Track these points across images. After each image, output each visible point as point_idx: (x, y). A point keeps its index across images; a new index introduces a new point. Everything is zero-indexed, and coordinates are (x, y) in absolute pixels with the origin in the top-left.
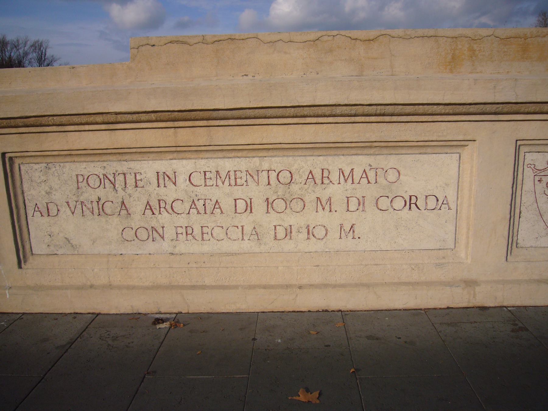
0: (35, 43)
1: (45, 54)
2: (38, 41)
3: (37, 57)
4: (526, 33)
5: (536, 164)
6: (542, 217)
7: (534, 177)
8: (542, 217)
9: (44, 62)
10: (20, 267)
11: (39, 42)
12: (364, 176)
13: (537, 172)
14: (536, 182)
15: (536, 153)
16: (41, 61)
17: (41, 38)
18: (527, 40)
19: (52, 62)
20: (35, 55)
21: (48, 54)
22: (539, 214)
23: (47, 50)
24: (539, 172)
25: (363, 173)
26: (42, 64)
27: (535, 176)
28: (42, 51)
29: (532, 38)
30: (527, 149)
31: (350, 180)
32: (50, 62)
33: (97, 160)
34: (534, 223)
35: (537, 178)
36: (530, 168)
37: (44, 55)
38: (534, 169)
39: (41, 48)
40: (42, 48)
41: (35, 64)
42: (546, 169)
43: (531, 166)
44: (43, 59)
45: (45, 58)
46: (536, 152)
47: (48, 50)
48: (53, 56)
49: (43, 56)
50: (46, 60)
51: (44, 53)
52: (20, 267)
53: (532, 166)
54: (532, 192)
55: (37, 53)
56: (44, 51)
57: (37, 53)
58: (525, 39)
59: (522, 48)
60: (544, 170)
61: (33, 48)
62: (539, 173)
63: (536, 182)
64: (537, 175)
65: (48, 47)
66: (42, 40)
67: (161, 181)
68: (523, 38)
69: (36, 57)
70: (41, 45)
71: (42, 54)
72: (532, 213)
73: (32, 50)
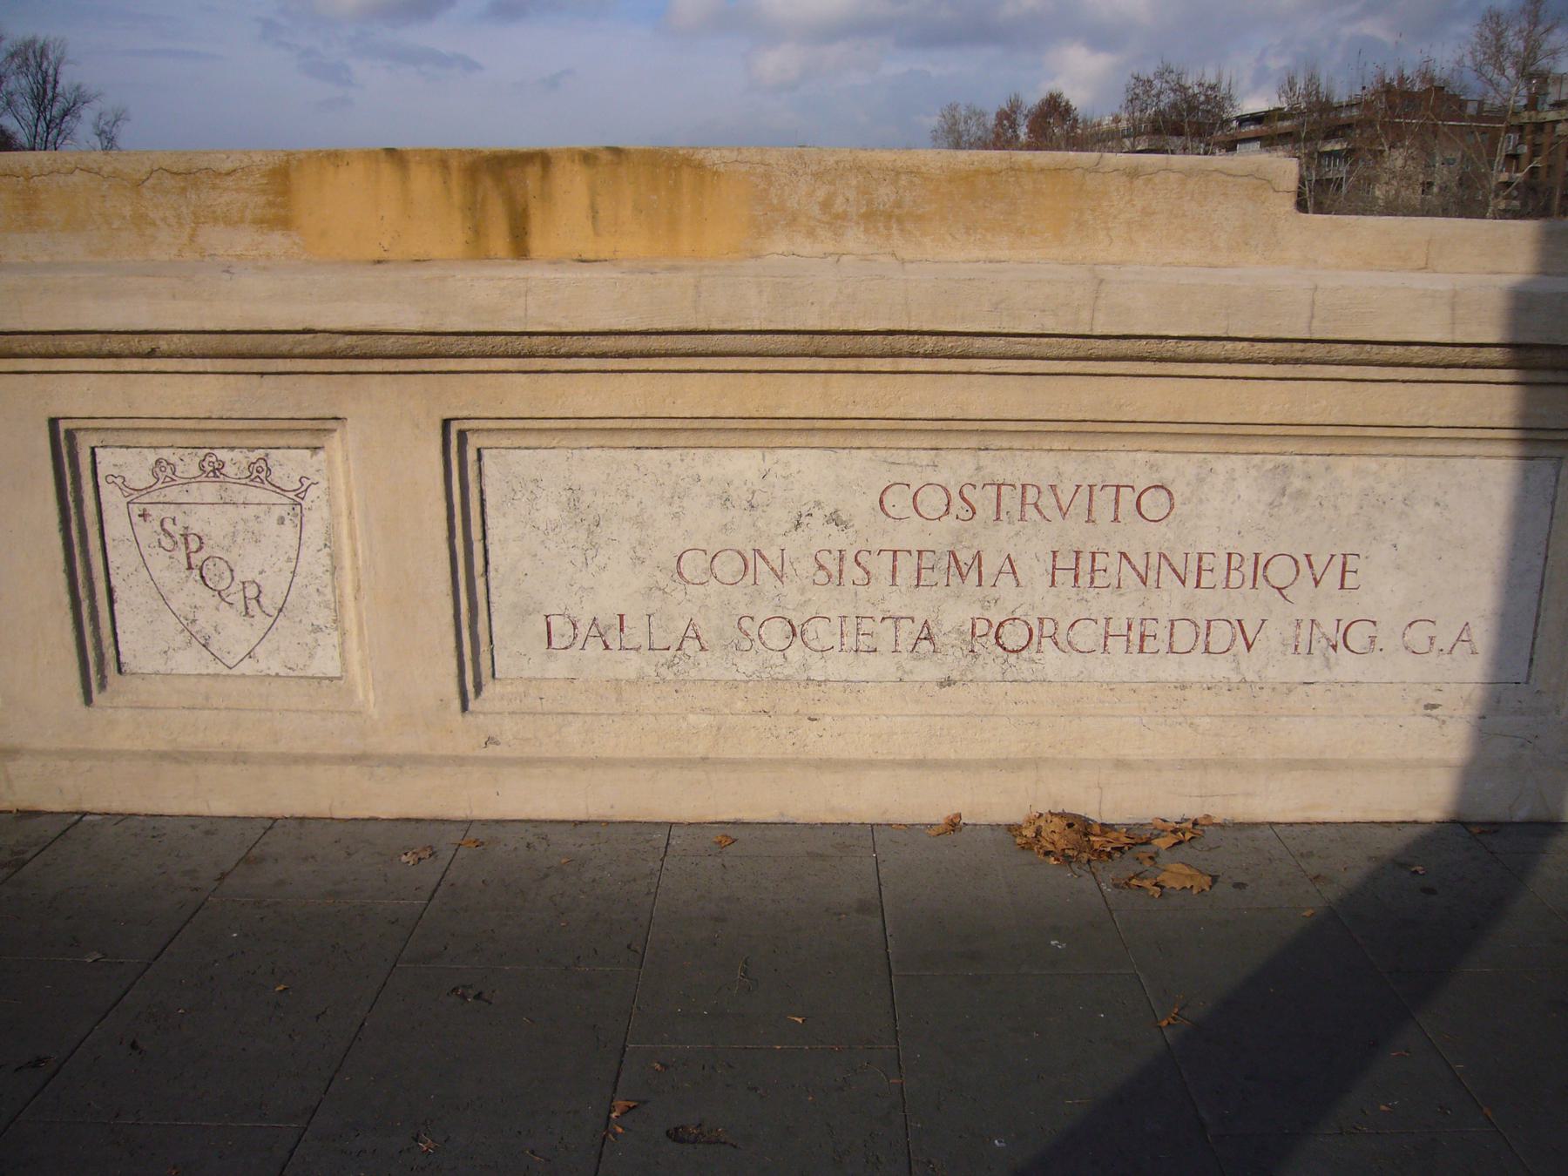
0: (25, 47)
1: (56, 82)
2: (33, 42)
3: (32, 90)
4: (26, 165)
5: (128, 475)
6: (166, 603)
7: (128, 508)
8: (166, 603)
9: (52, 106)
10: (88, 699)
11: (37, 46)
12: (1007, 567)
13: (131, 494)
14: (136, 519)
15: (122, 449)
16: (43, 101)
17: (42, 31)
18: (32, 181)
19: (77, 106)
20: (24, 82)
21: (63, 82)
22: (157, 596)
23: (59, 71)
24: (136, 494)
25: (1321, 578)
26: (45, 108)
27: (128, 503)
28: (46, 72)
29: (43, 177)
30: (94, 440)
31: (974, 576)
32: (71, 104)
33: (1215, 448)
34: (151, 616)
35: (136, 510)
36: (113, 484)
37: (53, 83)
38: (123, 487)
39: (42, 63)
40: (45, 65)
41: (27, 109)
42: (151, 487)
43: (116, 480)
44: (50, 94)
45: (54, 92)
46: (121, 447)
47: (64, 69)
48: (78, 88)
49: (49, 87)
50: (60, 99)
51: (51, 79)
52: (88, 699)
53: (119, 481)
54: (129, 543)
55: (31, 75)
56: (51, 72)
57: (30, 77)
58: (27, 179)
59: (24, 199)
60: (149, 490)
61: (17, 61)
62: (137, 498)
63: (136, 519)
64: (135, 501)
65: (65, 60)
66: (45, 41)
67: (1193, 566)
68: (22, 176)
69: (29, 90)
70: (43, 53)
71: (45, 82)
72: (141, 592)
73: (14, 66)
